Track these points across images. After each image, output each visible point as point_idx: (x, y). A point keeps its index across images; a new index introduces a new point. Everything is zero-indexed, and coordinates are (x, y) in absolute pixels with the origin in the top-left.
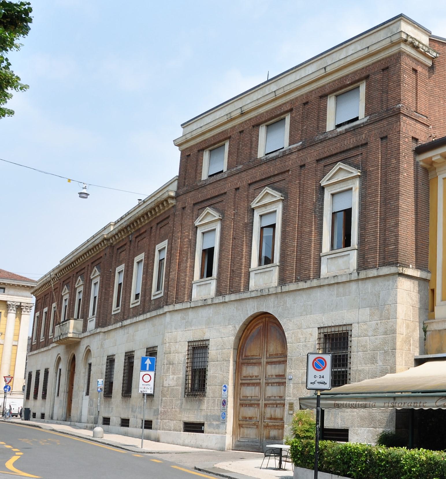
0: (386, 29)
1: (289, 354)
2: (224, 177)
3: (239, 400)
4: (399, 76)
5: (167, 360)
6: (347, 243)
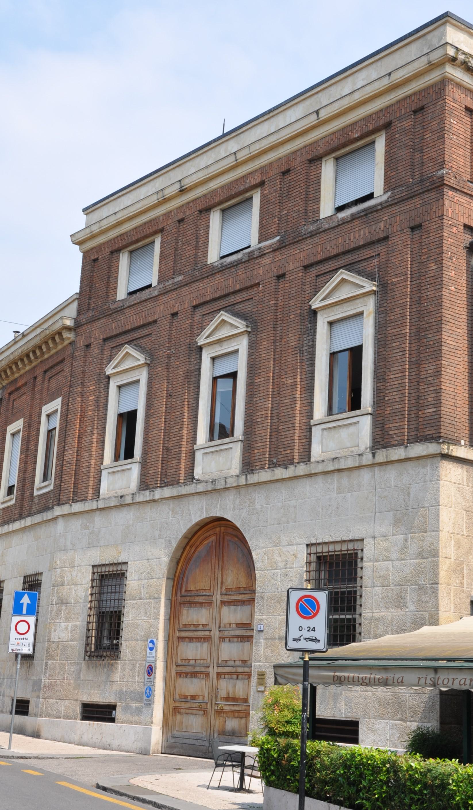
0: (421, 41)
1: (258, 589)
2: (154, 295)
3: (174, 667)
4: (442, 121)
5: (58, 597)
6: (355, 403)
